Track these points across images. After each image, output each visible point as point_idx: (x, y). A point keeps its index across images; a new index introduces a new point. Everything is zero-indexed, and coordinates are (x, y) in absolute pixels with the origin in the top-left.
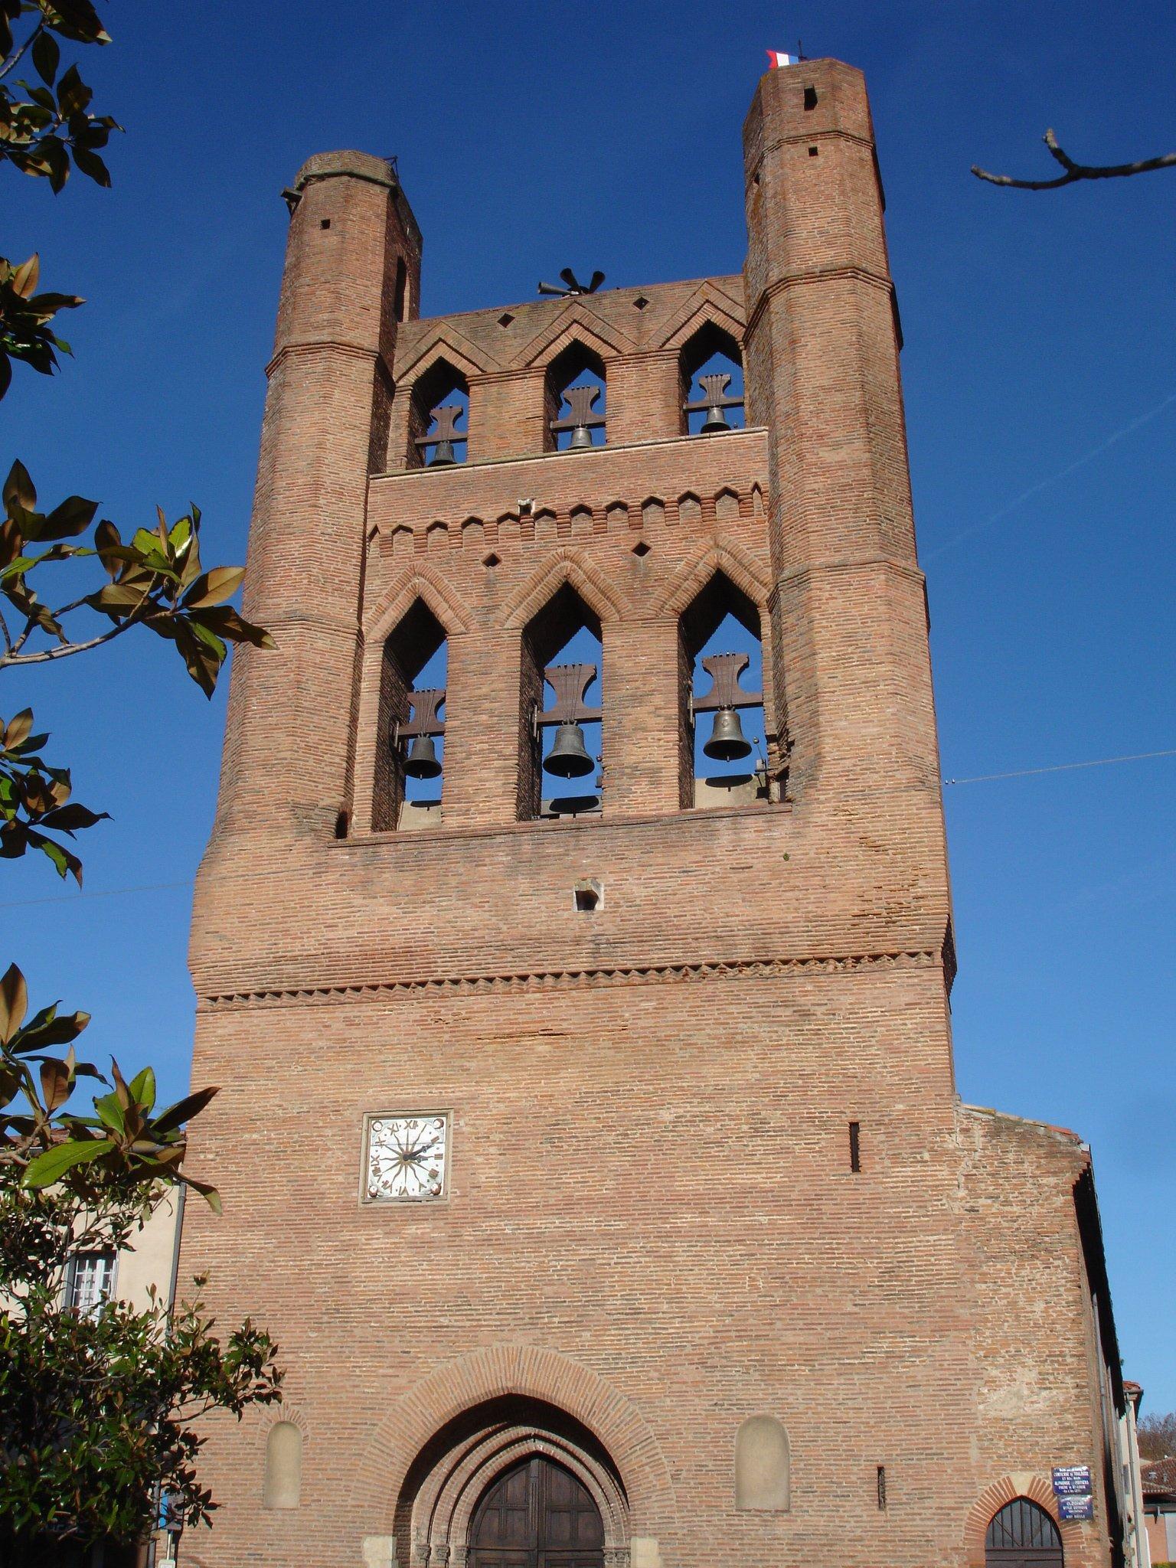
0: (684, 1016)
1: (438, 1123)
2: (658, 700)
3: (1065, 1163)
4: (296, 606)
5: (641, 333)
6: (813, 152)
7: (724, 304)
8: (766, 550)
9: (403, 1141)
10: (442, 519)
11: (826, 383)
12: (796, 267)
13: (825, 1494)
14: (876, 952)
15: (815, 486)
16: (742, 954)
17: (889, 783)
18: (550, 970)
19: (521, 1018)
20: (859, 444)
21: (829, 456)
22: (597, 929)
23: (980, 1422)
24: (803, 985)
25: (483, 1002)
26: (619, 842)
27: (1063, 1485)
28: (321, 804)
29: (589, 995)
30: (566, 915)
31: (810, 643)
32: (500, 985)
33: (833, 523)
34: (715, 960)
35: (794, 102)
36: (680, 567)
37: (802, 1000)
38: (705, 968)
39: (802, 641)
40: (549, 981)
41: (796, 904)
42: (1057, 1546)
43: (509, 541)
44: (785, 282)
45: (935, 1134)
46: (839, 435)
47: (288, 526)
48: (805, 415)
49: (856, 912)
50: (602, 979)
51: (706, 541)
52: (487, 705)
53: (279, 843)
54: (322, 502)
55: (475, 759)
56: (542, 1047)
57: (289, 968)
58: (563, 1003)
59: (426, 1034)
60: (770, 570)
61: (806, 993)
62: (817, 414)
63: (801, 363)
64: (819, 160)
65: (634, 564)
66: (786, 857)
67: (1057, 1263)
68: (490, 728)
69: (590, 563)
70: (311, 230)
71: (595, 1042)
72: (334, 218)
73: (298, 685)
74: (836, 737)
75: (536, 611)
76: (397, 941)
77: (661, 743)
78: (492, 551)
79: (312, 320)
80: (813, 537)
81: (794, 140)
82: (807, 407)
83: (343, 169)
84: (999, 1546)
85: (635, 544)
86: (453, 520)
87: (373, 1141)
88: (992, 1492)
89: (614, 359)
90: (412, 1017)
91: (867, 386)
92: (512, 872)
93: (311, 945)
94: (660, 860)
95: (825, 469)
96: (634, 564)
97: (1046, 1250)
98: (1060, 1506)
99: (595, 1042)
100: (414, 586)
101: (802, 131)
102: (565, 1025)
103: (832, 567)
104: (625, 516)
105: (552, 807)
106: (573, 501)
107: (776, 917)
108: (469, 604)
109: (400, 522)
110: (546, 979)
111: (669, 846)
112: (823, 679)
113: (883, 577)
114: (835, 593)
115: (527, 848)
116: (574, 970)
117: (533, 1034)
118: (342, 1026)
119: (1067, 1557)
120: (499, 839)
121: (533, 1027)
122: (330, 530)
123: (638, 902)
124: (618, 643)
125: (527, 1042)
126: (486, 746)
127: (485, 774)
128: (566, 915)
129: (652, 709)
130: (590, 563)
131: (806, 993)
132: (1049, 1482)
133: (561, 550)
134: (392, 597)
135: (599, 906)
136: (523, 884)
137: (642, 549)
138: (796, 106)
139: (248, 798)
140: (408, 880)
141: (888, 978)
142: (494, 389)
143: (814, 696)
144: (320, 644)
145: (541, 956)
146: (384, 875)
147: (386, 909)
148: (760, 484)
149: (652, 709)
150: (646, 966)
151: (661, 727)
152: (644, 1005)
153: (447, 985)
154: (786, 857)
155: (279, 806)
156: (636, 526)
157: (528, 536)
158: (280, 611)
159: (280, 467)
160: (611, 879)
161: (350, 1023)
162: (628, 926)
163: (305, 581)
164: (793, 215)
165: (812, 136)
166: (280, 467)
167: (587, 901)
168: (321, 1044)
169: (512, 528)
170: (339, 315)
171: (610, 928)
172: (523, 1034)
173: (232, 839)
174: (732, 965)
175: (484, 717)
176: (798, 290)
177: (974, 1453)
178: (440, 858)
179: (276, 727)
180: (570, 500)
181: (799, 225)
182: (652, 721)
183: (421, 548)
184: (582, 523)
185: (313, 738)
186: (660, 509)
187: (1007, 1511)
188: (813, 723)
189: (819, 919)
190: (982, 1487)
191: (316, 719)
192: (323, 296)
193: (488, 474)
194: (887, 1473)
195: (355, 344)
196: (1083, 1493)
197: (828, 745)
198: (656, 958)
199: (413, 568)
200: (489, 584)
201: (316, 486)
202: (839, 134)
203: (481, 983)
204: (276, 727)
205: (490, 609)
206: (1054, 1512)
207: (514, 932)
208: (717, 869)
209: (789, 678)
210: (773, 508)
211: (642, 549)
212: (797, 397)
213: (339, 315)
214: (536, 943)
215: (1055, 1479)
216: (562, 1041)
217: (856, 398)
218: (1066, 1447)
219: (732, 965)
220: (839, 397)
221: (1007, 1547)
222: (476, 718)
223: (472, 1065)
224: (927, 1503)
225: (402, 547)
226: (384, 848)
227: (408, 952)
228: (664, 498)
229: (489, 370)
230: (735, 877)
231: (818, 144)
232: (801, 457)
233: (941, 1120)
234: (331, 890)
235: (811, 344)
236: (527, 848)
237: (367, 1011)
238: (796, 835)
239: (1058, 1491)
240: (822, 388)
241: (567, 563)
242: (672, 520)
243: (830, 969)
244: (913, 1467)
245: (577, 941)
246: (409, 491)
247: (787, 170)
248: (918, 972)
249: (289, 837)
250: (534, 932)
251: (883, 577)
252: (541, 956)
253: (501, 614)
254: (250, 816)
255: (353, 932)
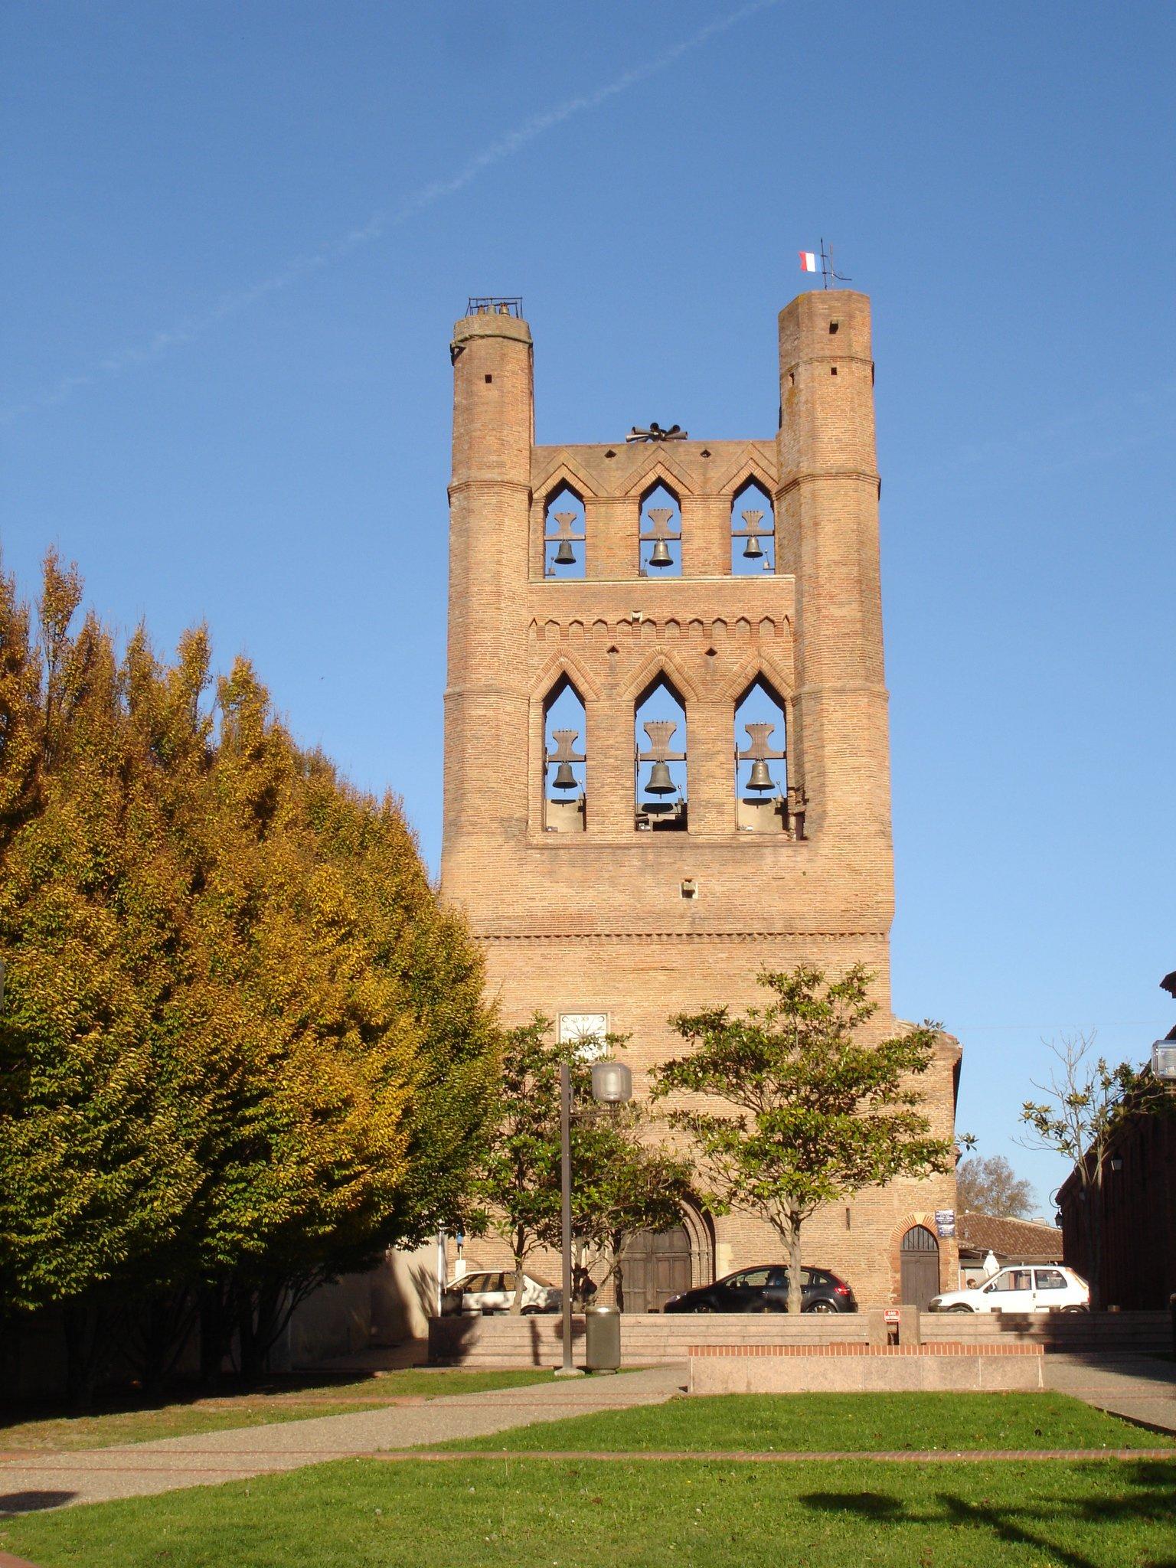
0: (743, 963)
1: (602, 1019)
2: (722, 758)
3: (950, 1054)
4: (491, 682)
5: (706, 481)
6: (834, 371)
7: (763, 463)
8: (791, 662)
9: (581, 1028)
10: (580, 619)
11: (837, 558)
12: (820, 466)
13: (819, 1222)
14: (854, 931)
15: (827, 632)
16: (778, 928)
17: (865, 832)
18: (665, 932)
19: (649, 960)
20: (855, 605)
21: (836, 612)
22: (694, 910)
23: (899, 1187)
24: (811, 948)
25: (624, 949)
26: (705, 857)
27: (940, 1219)
28: (516, 816)
29: (688, 948)
30: (675, 900)
31: (821, 739)
32: (636, 940)
33: (837, 659)
34: (762, 931)
35: (822, 325)
36: (736, 668)
37: (810, 957)
38: (756, 936)
39: (815, 736)
40: (665, 938)
41: (809, 901)
42: (936, 1249)
43: (624, 639)
44: (812, 477)
45: (881, 1035)
46: (843, 597)
47: (482, 622)
48: (822, 581)
49: (843, 909)
50: (696, 939)
51: (752, 651)
52: (613, 752)
53: (494, 844)
54: (503, 605)
55: (607, 788)
56: (662, 977)
57: (506, 923)
58: (673, 951)
59: (592, 966)
60: (793, 676)
61: (813, 953)
62: (830, 579)
63: (821, 542)
64: (838, 379)
65: (706, 662)
66: (804, 873)
67: (942, 1106)
68: (616, 768)
69: (678, 660)
70: (478, 382)
71: (692, 975)
72: (494, 374)
73: (497, 737)
74: (835, 801)
75: (642, 689)
76: (573, 910)
77: (724, 786)
78: (613, 644)
79: (485, 460)
80: (825, 668)
81: (821, 360)
82: (824, 575)
83: (497, 332)
84: (906, 1249)
85: (707, 649)
86: (588, 619)
87: (562, 1028)
88: (905, 1222)
89: (688, 497)
90: (582, 956)
91: (862, 563)
92: (642, 871)
93: (519, 909)
94: (731, 870)
95: (835, 621)
96: (706, 662)
97: (938, 1100)
98: (939, 1229)
99: (692, 975)
100: (561, 664)
101: (827, 353)
102: (675, 965)
103: (836, 691)
104: (701, 628)
105: (643, 809)
106: (668, 616)
107: (798, 908)
108: (599, 680)
109: (550, 617)
110: (662, 937)
111: (735, 862)
112: (828, 763)
113: (866, 700)
114: (837, 708)
115: (651, 857)
116: (679, 933)
117: (655, 969)
118: (540, 959)
119: (941, 1255)
120: (633, 851)
121: (655, 965)
122: (509, 626)
123: (718, 895)
124: (697, 717)
125: (651, 973)
126: (614, 780)
127: (613, 799)
128: (675, 900)
129: (719, 764)
130: (678, 660)
131: (813, 953)
132: (933, 1217)
133: (658, 647)
134: (546, 670)
135: (695, 896)
136: (649, 879)
137: (711, 652)
138: (822, 329)
139: (471, 812)
140: (578, 873)
141: (859, 946)
142: (603, 509)
143: (822, 774)
144: (509, 709)
145: (659, 924)
146: (563, 869)
147: (565, 890)
148: (789, 616)
149: (719, 764)
150: (722, 932)
151: (723, 776)
152: (720, 955)
153: (604, 937)
154: (804, 873)
155: (492, 819)
156: (707, 635)
157: (636, 636)
158: (482, 684)
159: (472, 576)
160: (702, 880)
161: (545, 957)
162: (711, 909)
163: (497, 664)
164: (818, 423)
165: (834, 358)
166: (472, 576)
167: (688, 894)
168: (527, 969)
169: (625, 628)
170: (504, 458)
171: (701, 910)
172: (650, 969)
173: (463, 839)
174: (770, 934)
175: (612, 760)
176: (821, 484)
177: (896, 1203)
178: (597, 860)
179: (485, 766)
180: (665, 614)
181: (823, 432)
182: (718, 772)
183: (565, 636)
184: (673, 631)
185: (509, 773)
186: (724, 626)
187: (911, 1231)
188: (821, 789)
189: (823, 912)
190: (899, 1220)
191: (509, 760)
192: (491, 440)
193: (610, 588)
194: (851, 1211)
195: (516, 482)
196: (950, 1223)
197: (830, 807)
198: (727, 928)
199: (560, 651)
200: (612, 668)
201: (498, 593)
202: (852, 358)
203: (624, 937)
204: (485, 766)
205: (614, 686)
206: (935, 1233)
207: (645, 909)
208: (764, 878)
209: (807, 758)
210: (798, 636)
211: (711, 652)
212: (817, 566)
213: (504, 458)
214: (659, 916)
215: (937, 1216)
216: (673, 974)
217: (855, 571)
218: (942, 1201)
219: (770, 934)
220: (844, 570)
221: (911, 1249)
222: (606, 761)
223: (620, 985)
224: (871, 1227)
225: (552, 635)
226: (562, 851)
227: (580, 917)
228: (727, 620)
229: (600, 495)
230: (775, 884)
231: (837, 365)
232: (819, 610)
233: (885, 1028)
234: (529, 876)
235: (828, 528)
236: (651, 857)
237: (554, 951)
238: (810, 861)
239: (938, 1222)
240: (834, 562)
241: (662, 657)
242: (731, 634)
243: (827, 940)
244: (865, 1208)
245: (682, 917)
246: (556, 596)
247: (816, 384)
248: (876, 944)
249: (500, 840)
250: (656, 909)
251: (866, 700)
252: (659, 924)
253: (621, 689)
254: (474, 824)
255: (545, 904)
